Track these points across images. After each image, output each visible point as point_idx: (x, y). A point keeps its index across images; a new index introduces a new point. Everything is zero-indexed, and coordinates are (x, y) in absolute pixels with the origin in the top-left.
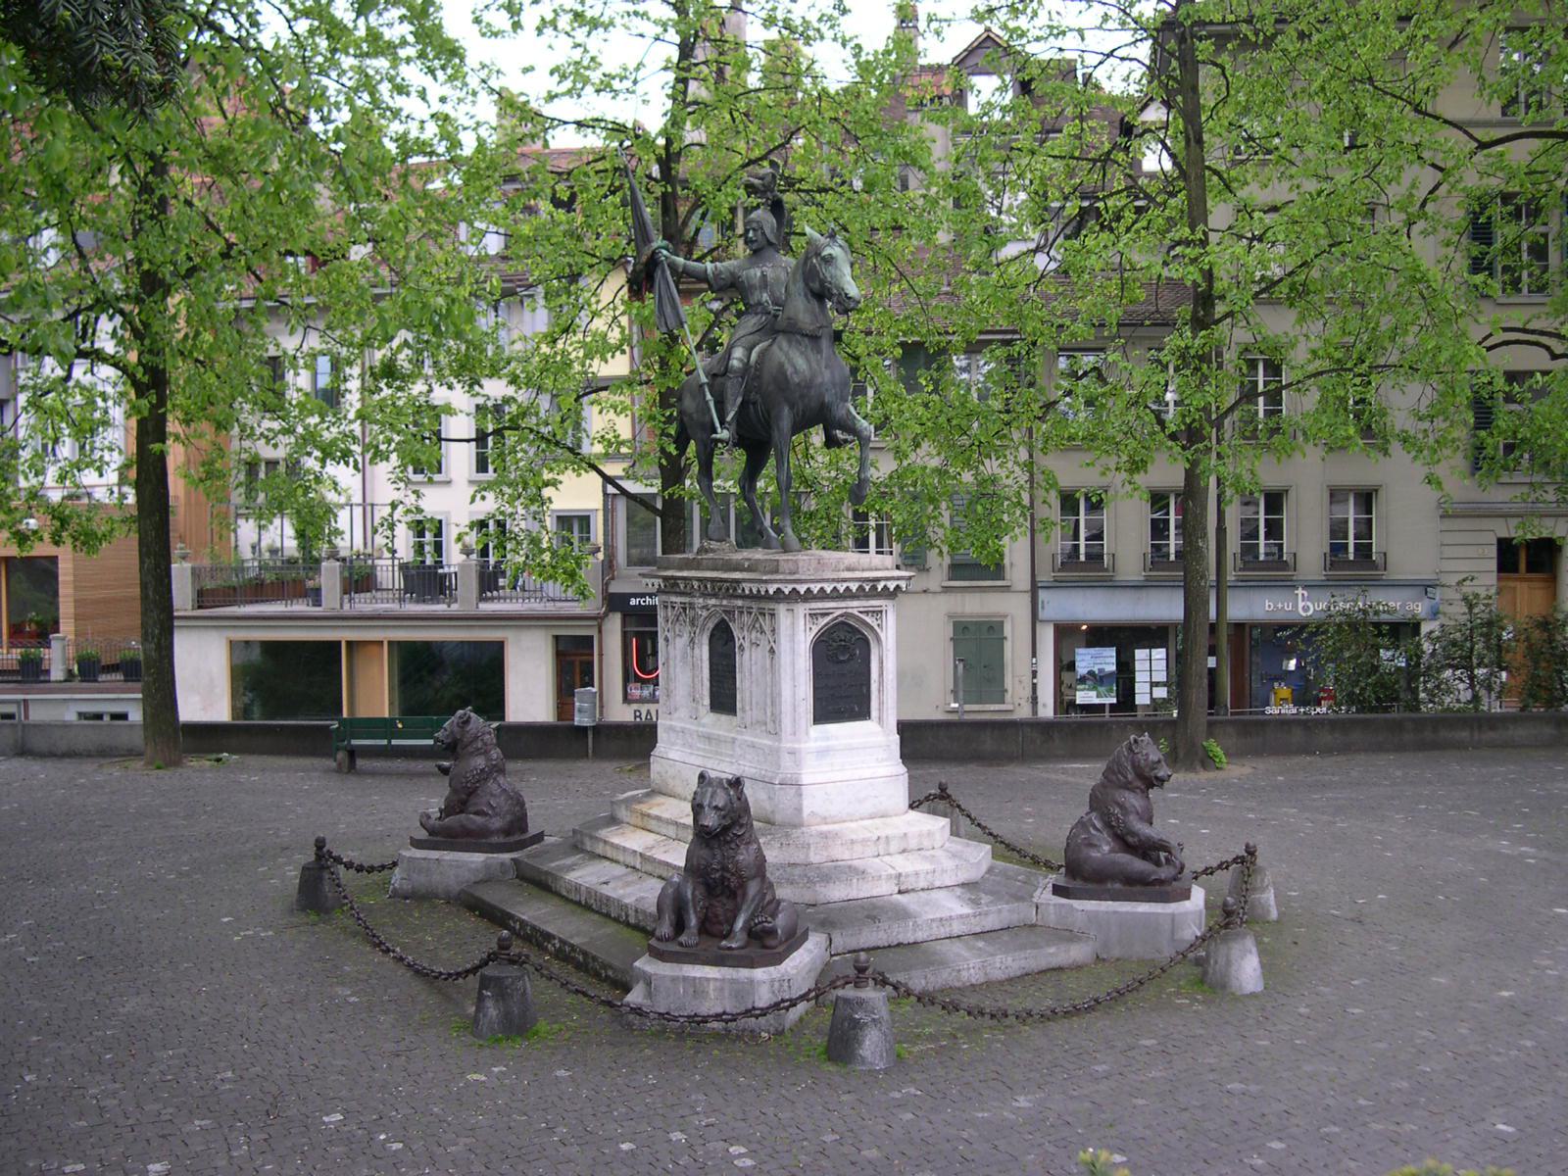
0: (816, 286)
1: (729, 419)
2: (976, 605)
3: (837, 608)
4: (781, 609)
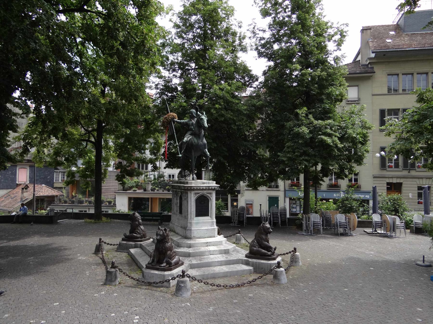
2: (273, 193)
3: (201, 192)
4: (189, 192)
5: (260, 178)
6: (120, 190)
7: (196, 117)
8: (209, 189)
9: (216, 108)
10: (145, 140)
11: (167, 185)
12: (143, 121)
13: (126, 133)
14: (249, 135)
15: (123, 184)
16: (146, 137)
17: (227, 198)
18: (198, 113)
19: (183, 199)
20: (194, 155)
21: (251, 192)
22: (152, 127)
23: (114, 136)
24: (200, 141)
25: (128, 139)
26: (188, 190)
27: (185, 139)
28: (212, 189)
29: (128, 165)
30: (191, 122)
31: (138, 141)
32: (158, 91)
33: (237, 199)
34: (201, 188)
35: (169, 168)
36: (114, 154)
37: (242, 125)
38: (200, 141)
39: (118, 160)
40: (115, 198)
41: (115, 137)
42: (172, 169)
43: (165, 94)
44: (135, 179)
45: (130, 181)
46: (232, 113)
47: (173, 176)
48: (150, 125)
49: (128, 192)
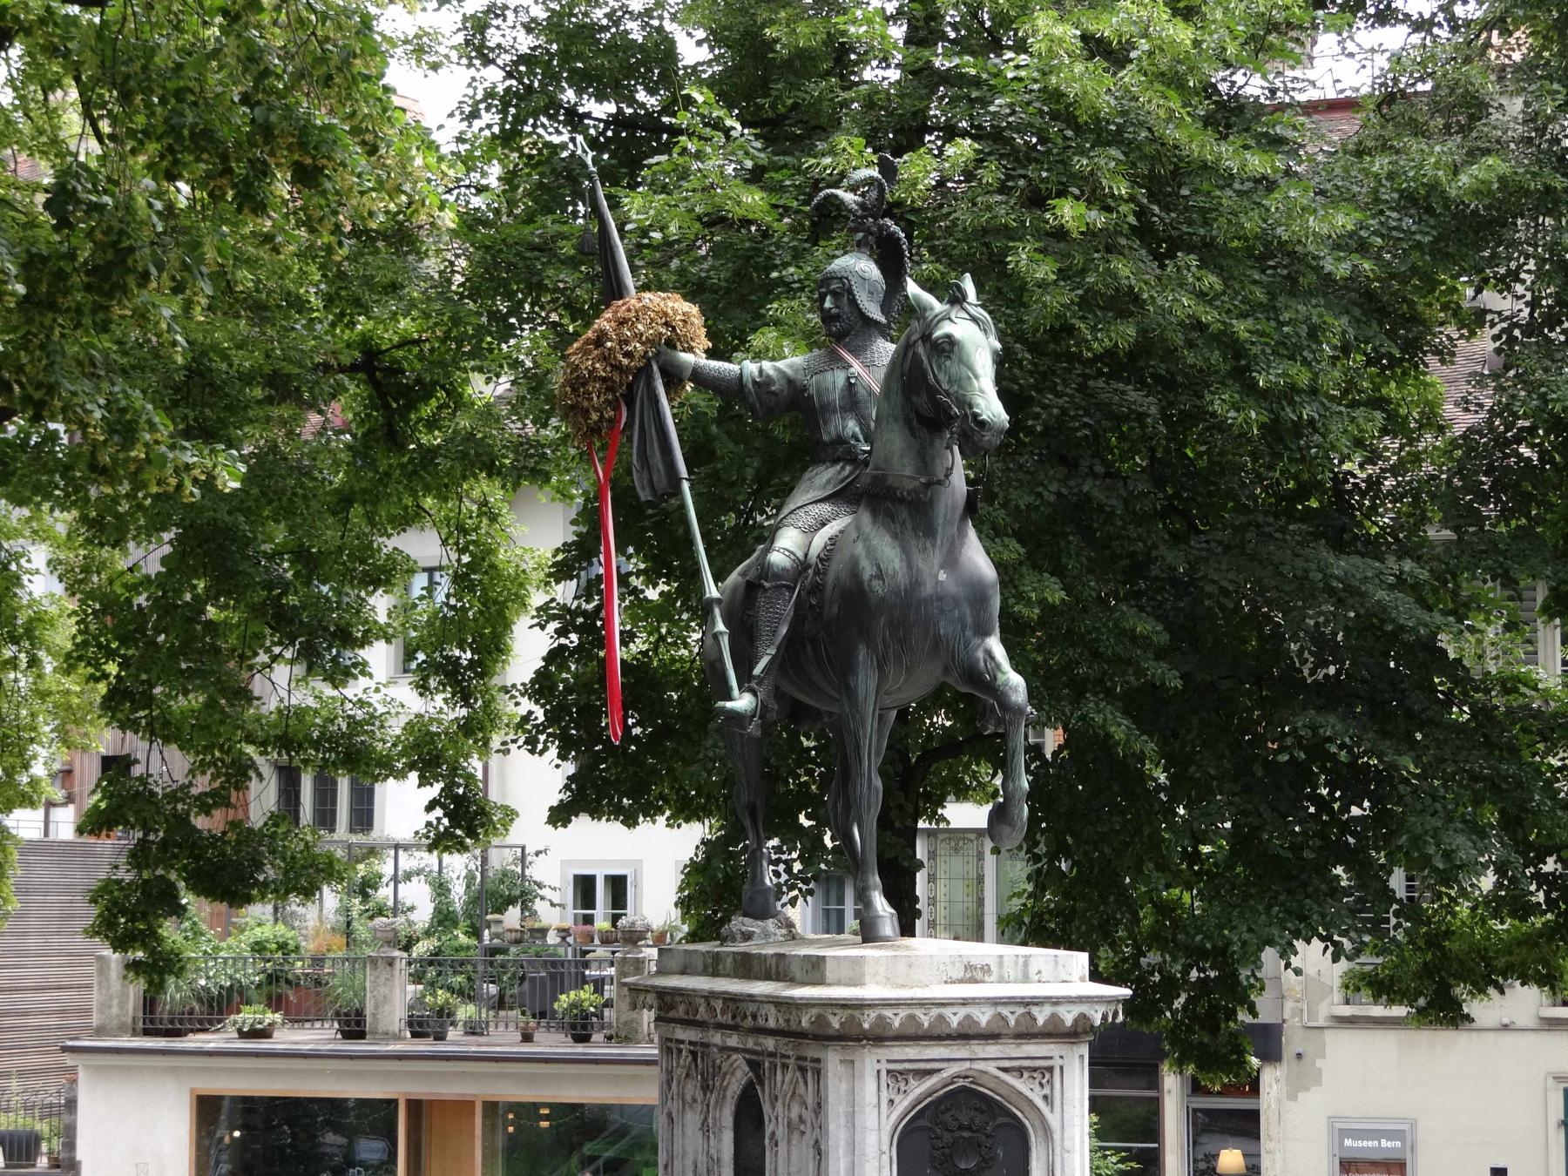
0: (921, 401)
1: (757, 671)
4: (833, 1060)
5: (1496, 905)
6: (121, 1030)
7: (884, 331)
8: (1027, 1025)
9: (1060, 233)
10: (368, 549)
11: (563, 973)
12: (352, 369)
13: (209, 485)
14: (1374, 483)
15: (157, 968)
16: (370, 519)
17: (1154, 1109)
18: (912, 288)
19: (775, 1125)
20: (875, 695)
21: (1386, 1044)
22: (432, 424)
23: (70, 516)
24: (937, 557)
25: (211, 543)
26: (822, 1036)
27: (787, 546)
28: (1055, 1033)
29: (202, 784)
30: (840, 378)
31: (301, 556)
32: (493, 75)
33: (1254, 1116)
34: (954, 1019)
35: (595, 814)
36: (72, 684)
37: (1314, 391)
38: (937, 557)
39: (106, 739)
40: (71, 1105)
41: (84, 519)
42: (630, 822)
43: (552, 107)
44: (259, 919)
45: (215, 941)
46: (1212, 280)
47: (618, 886)
48: (411, 406)
49: (193, 1042)
